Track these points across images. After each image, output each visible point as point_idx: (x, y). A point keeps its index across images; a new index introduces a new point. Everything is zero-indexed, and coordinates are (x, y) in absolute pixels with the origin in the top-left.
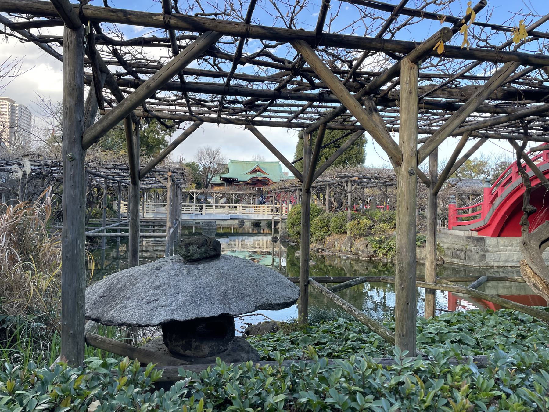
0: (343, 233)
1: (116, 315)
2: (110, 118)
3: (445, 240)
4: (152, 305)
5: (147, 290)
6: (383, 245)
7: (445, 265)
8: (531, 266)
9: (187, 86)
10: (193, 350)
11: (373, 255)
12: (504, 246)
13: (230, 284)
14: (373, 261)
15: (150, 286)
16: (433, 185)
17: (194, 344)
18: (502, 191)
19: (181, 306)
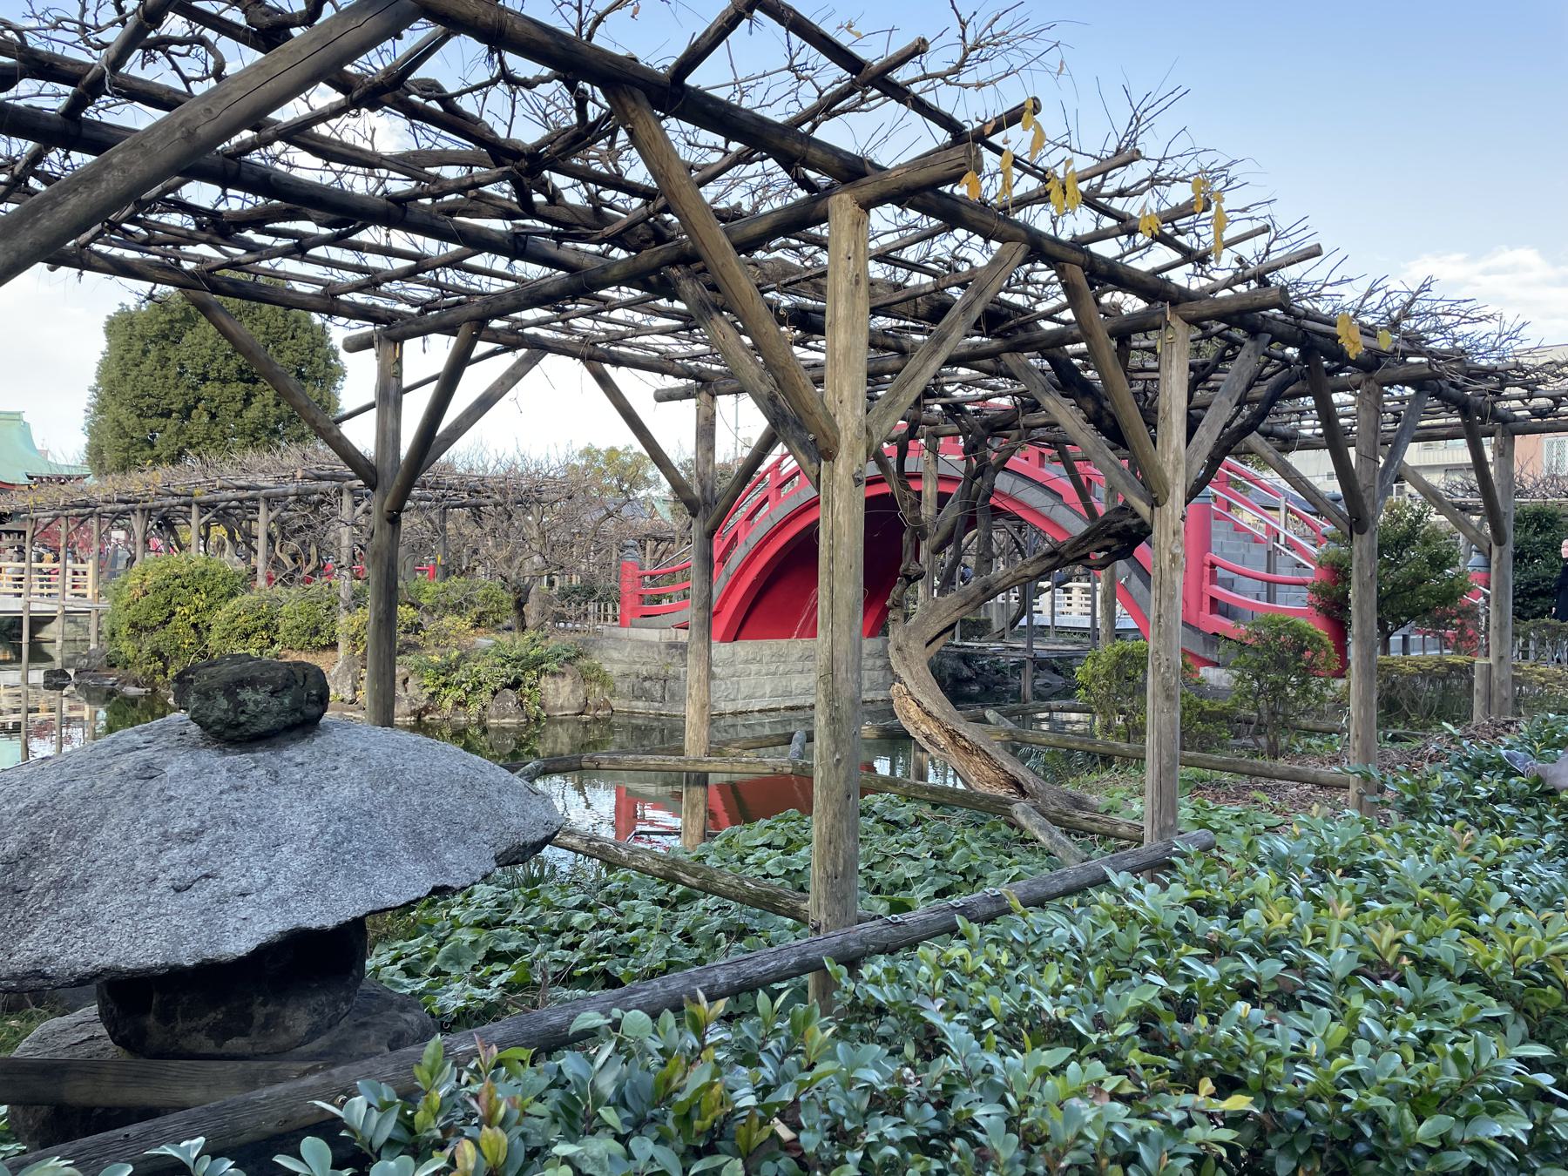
0: (324, 648)
1: (55, 950)
2: (45, 223)
3: (615, 655)
4: (202, 895)
5: (153, 849)
6: (456, 676)
7: (614, 719)
8: (918, 696)
9: (86, 132)
10: (254, 1034)
11: (426, 710)
12: (746, 662)
13: (416, 801)
14: (427, 725)
15: (164, 834)
16: (706, 511)
17: (260, 1013)
18: (748, 528)
19: (310, 883)
